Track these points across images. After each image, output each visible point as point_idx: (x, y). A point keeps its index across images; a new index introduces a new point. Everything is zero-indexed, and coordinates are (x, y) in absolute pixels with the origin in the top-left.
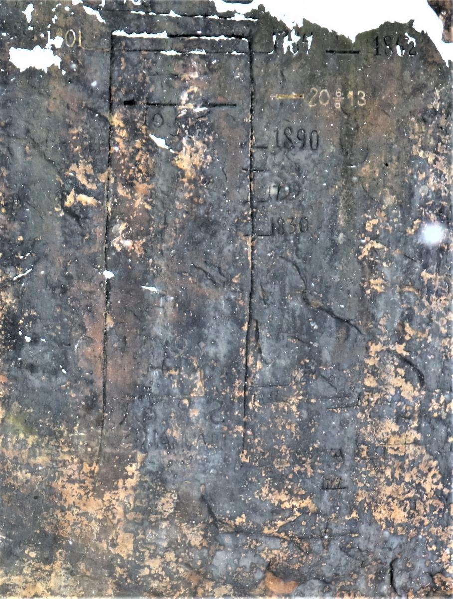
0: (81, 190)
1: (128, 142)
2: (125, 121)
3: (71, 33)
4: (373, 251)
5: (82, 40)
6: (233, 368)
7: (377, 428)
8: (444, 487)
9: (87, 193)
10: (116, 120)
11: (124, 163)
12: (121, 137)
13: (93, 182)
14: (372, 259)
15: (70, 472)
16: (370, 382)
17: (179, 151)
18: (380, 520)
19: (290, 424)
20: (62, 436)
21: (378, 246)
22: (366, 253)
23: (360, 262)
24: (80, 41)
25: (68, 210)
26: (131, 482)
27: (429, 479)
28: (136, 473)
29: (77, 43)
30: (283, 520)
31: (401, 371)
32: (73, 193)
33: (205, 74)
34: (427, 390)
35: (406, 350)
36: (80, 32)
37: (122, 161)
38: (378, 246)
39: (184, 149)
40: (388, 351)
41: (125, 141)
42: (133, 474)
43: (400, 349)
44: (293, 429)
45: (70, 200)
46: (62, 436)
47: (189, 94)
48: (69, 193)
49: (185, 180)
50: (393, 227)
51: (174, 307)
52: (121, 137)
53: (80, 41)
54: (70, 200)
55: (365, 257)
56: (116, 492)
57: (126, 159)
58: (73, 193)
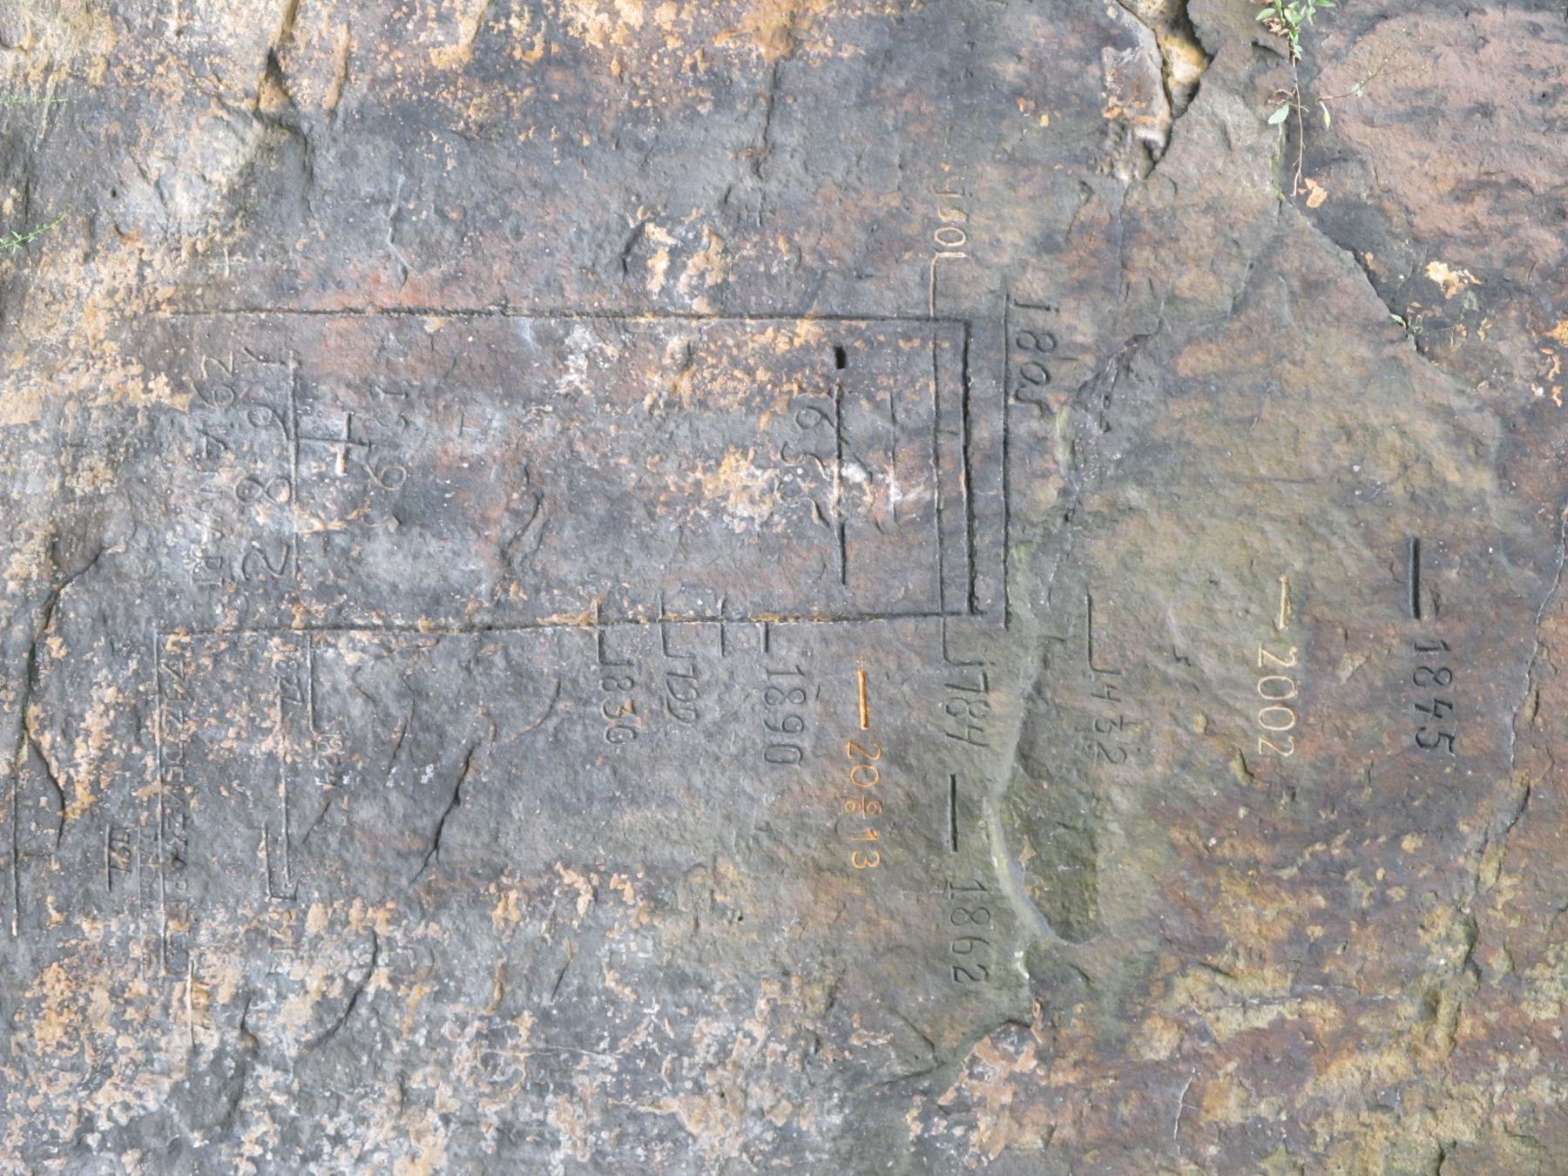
0: (677, 255)
1: (766, 352)
2: (806, 348)
3: (960, 239)
4: (572, 894)
5: (947, 259)
6: (345, 596)
7: (225, 946)
8: (103, 1133)
9: (673, 272)
10: (806, 329)
11: (728, 347)
12: (775, 339)
13: (690, 285)
14: (556, 893)
15: (157, 264)
16: (315, 919)
17: (752, 462)
18: (42, 984)
19: (238, 737)
20: (225, 234)
21: (583, 903)
22: (567, 881)
23: (549, 867)
24: (947, 254)
25: (639, 231)
26: (135, 386)
27: (118, 1097)
28: (153, 397)
29: (942, 250)
30: (53, 747)
31: (336, 991)
32: (671, 241)
33: (896, 517)
34: (300, 1060)
35: (379, 993)
36: (963, 255)
37: (730, 342)
38: (583, 903)
39: (758, 473)
40: (377, 950)
41: (765, 348)
42: (151, 391)
43: (381, 979)
44: (226, 744)
45: (656, 233)
46: (225, 234)
47: (859, 486)
48: (670, 233)
49: (699, 475)
50: (619, 942)
51: (463, 459)
52: (775, 339)
53: (947, 254)
54: (656, 233)
55: (560, 877)
56: (118, 364)
57: (735, 351)
58: (671, 241)
